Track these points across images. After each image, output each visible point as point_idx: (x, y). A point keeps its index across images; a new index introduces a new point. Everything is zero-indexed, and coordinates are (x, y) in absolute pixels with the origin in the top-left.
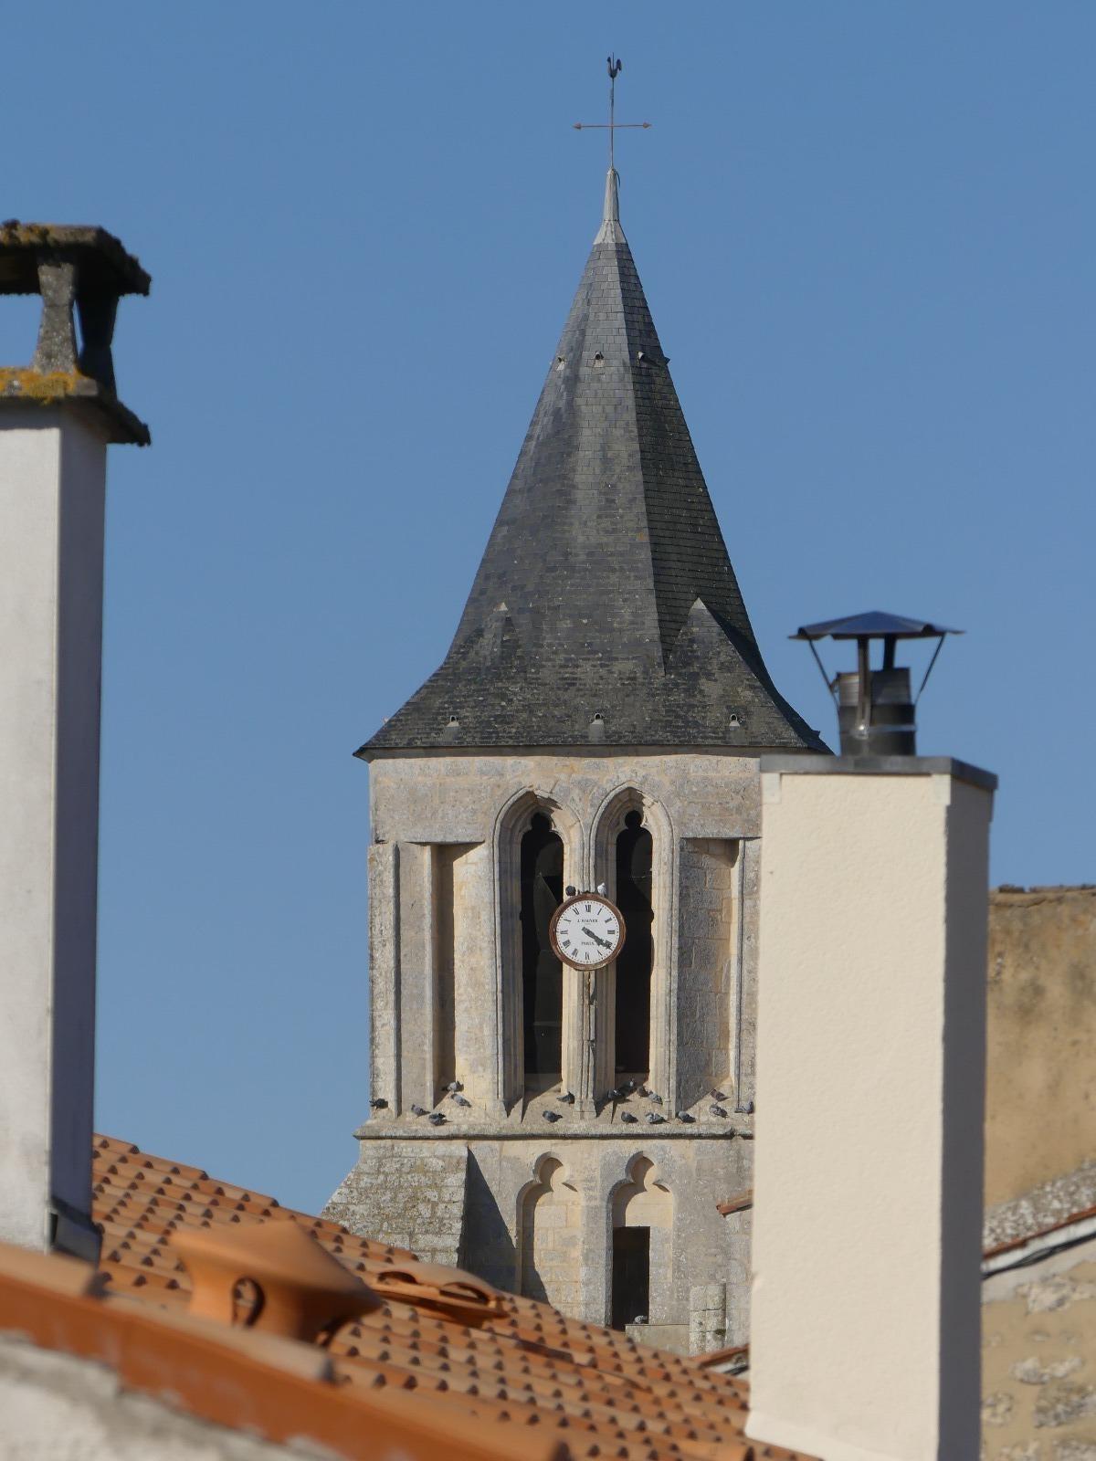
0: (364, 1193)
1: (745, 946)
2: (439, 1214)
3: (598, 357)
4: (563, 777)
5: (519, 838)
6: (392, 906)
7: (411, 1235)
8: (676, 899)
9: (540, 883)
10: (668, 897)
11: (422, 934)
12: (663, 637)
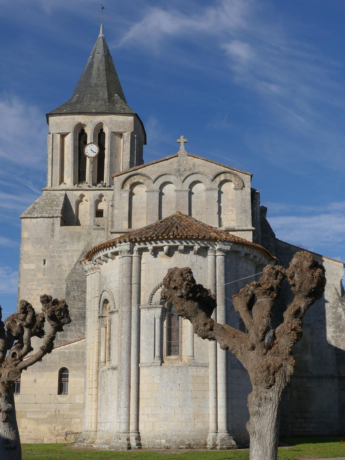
0: (43, 200)
1: (124, 153)
2: (58, 203)
3: (98, 53)
4: (87, 120)
5: (78, 133)
6: (74, 192)
7: (52, 207)
8: (110, 144)
9: (82, 141)
10: (108, 143)
11: (58, 151)
12: (108, 98)
